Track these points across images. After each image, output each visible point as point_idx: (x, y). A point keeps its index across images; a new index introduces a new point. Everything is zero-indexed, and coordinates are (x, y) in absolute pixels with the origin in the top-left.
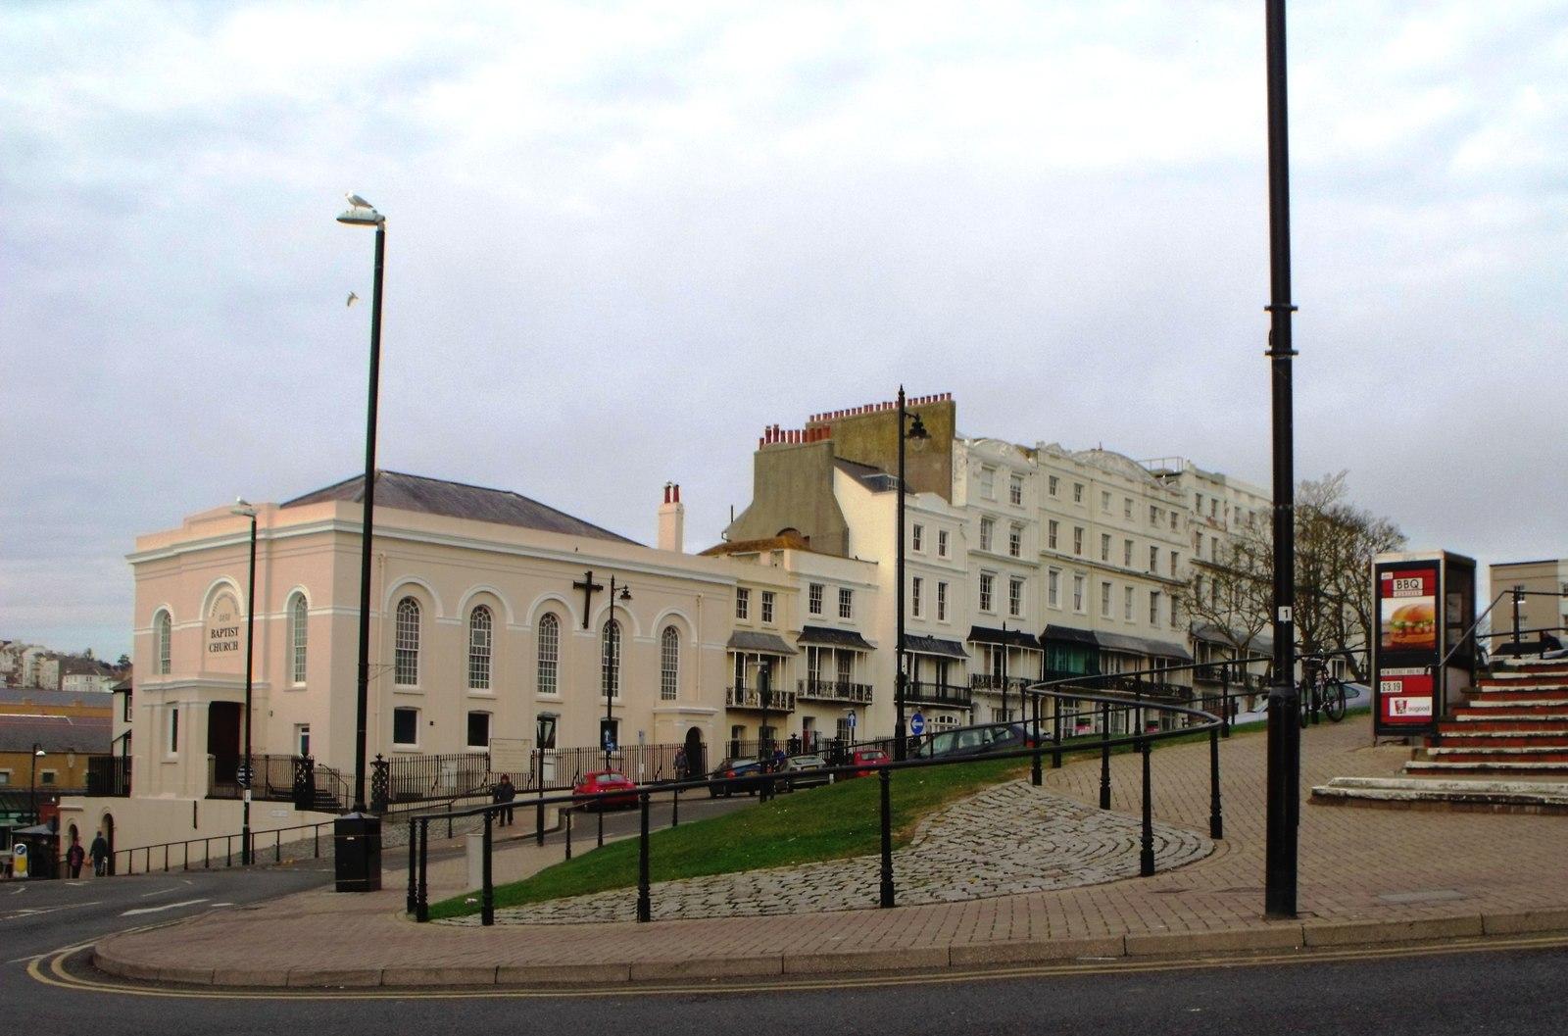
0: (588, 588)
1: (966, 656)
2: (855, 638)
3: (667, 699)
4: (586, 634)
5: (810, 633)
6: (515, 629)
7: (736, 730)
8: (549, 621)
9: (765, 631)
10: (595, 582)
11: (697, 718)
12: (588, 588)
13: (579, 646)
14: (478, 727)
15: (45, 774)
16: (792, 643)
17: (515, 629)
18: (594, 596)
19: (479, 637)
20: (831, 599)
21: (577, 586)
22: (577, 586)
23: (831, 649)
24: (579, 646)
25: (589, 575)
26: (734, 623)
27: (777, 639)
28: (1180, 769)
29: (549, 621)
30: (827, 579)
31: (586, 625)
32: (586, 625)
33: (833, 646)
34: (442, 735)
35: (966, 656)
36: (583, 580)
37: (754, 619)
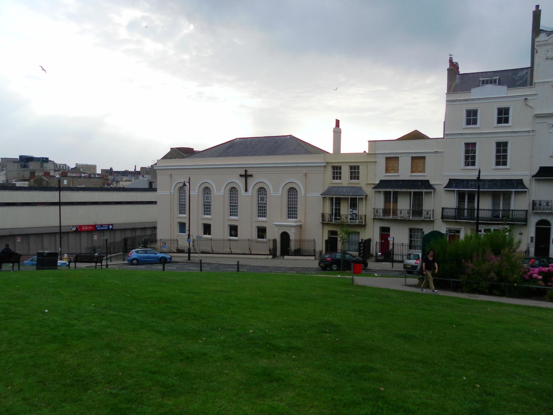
0: (246, 176)
1: (527, 189)
2: (426, 184)
6: (220, 194)
8: (233, 190)
9: (350, 185)
10: (249, 173)
11: (285, 228)
12: (246, 176)
13: (247, 200)
14: (234, 230)
15: (263, 238)
16: (369, 191)
17: (220, 194)
18: (249, 179)
19: (208, 198)
20: (346, 172)
21: (241, 176)
22: (241, 176)
23: (391, 192)
24: (247, 200)
27: (360, 188)
28: (356, 254)
29: (233, 190)
30: (399, 153)
31: (246, 190)
32: (246, 190)
33: (391, 190)
34: (220, 232)
35: (527, 189)
36: (243, 173)
37: (345, 180)
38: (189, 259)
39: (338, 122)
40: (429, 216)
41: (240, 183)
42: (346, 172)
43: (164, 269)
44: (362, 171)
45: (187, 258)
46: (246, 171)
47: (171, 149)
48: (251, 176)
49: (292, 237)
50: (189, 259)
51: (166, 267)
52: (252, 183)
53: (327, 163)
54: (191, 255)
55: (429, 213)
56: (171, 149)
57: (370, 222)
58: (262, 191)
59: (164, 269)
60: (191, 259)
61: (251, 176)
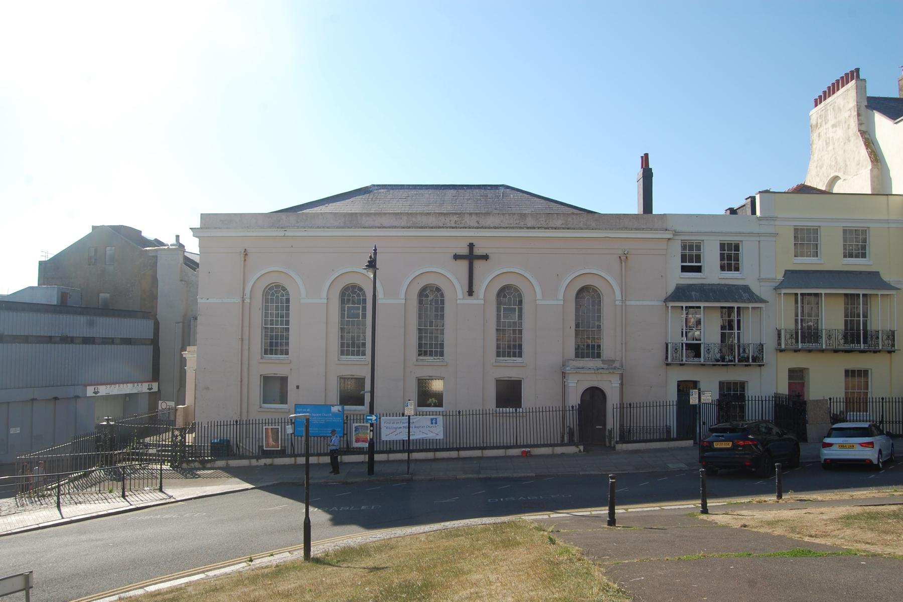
3: (583, 357)
4: (470, 301)
5: (793, 277)
7: (684, 388)
10: (465, 251)
12: (471, 257)
17: (395, 301)
18: (478, 265)
20: (711, 258)
22: (457, 257)
25: (471, 246)
26: (677, 278)
29: (430, 299)
31: (471, 292)
32: (471, 292)
38: (371, 471)
39: (645, 159)
40: (746, 355)
41: (452, 279)
42: (711, 258)
43: (612, 522)
44: (747, 256)
45: (365, 469)
46: (471, 246)
47: (94, 228)
48: (485, 257)
49: (613, 399)
50: (371, 471)
51: (619, 510)
52: (488, 278)
53: (676, 233)
54: (377, 457)
55: (747, 351)
56: (94, 228)
57: (769, 355)
58: (509, 298)
59: (612, 522)
60: (376, 468)
61: (485, 257)
